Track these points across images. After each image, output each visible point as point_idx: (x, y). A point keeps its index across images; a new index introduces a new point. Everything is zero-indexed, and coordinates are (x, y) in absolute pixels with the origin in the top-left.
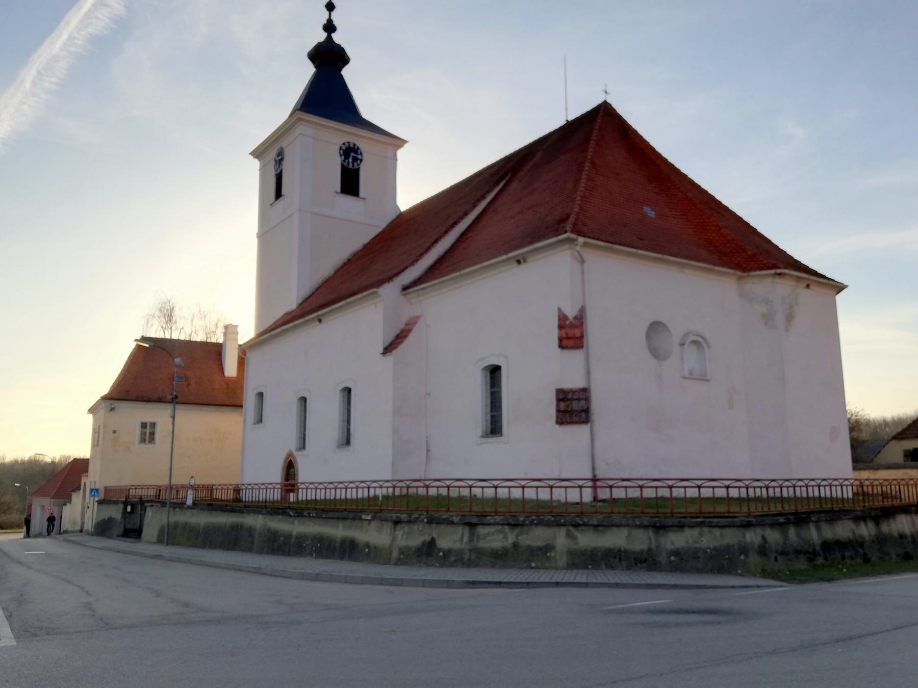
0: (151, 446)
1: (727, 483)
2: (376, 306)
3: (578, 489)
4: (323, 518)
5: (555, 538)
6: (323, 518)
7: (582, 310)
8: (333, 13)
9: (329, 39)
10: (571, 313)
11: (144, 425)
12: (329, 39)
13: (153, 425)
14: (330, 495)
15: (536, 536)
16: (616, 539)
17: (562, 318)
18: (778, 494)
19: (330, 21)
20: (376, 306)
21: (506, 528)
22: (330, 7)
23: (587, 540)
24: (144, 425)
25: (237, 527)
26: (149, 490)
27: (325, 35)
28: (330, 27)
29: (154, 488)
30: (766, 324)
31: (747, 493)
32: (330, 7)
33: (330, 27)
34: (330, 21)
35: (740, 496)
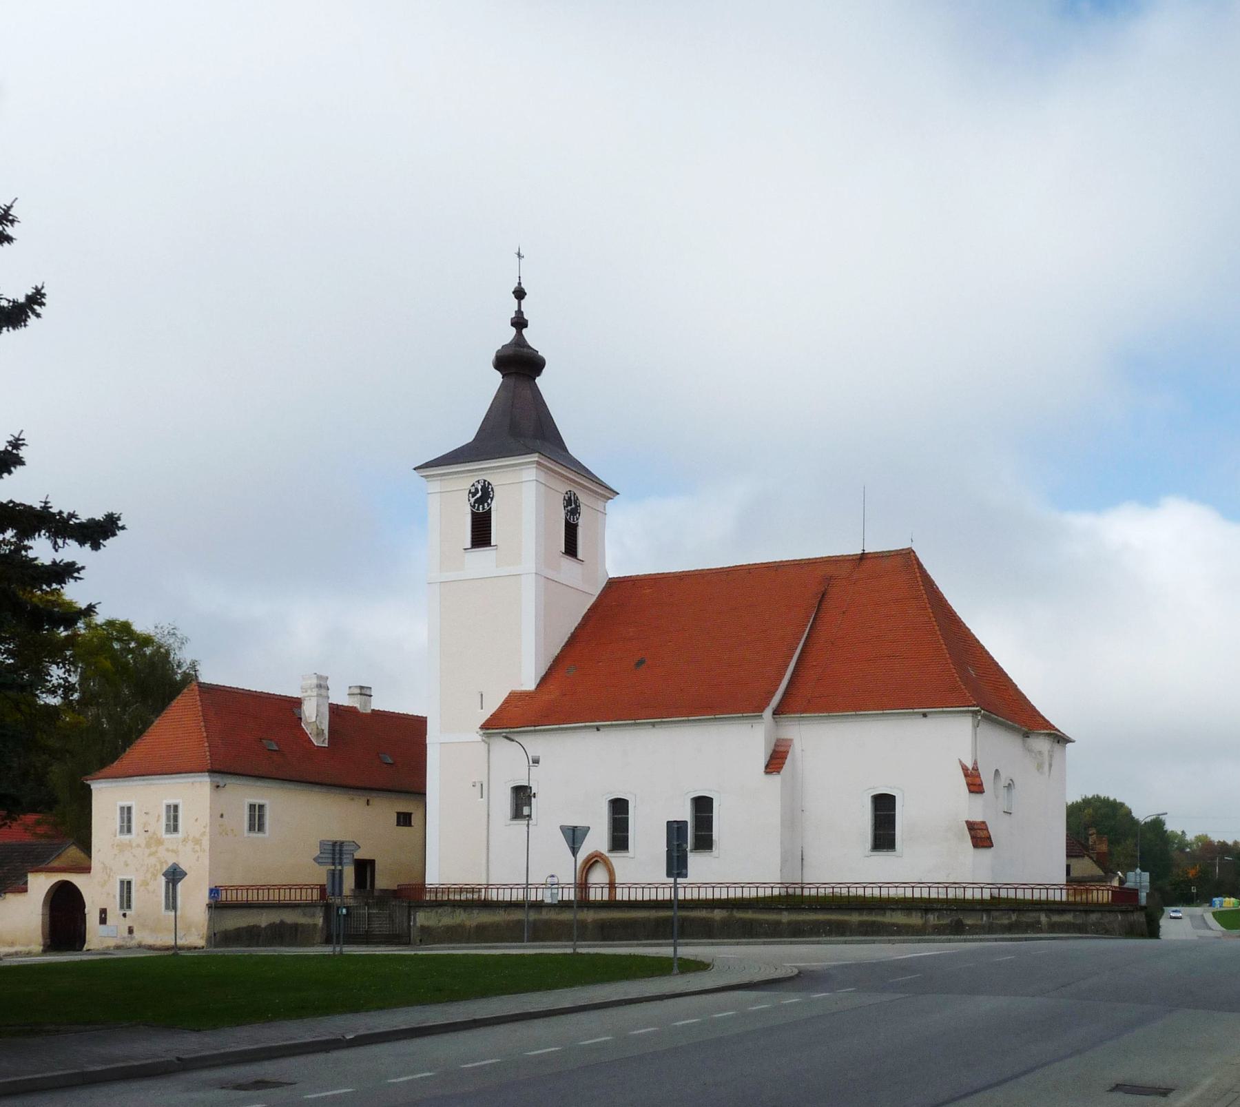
0: (260, 835)
1: (643, 886)
2: (752, 726)
3: (1031, 890)
4: (832, 909)
5: (1039, 918)
6: (832, 909)
7: (975, 763)
8: (523, 302)
9: (519, 341)
10: (970, 766)
11: (252, 807)
12: (519, 341)
13: (261, 807)
14: (960, 894)
15: (1029, 918)
16: (1068, 918)
17: (965, 769)
18: (942, 896)
19: (519, 313)
20: (752, 726)
21: (1011, 912)
22: (520, 294)
23: (1056, 918)
24: (252, 807)
25: (296, 930)
26: (1100, 892)
27: (513, 331)
28: (519, 323)
29: (1108, 890)
30: (1038, 770)
31: (802, 892)
32: (520, 294)
33: (519, 323)
34: (519, 313)
35: (602, 900)
